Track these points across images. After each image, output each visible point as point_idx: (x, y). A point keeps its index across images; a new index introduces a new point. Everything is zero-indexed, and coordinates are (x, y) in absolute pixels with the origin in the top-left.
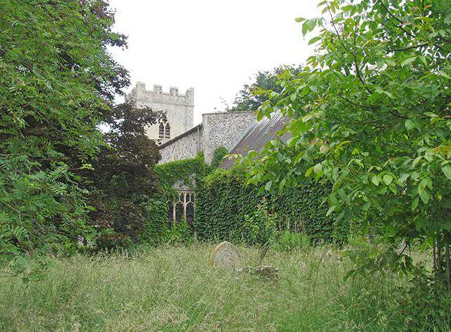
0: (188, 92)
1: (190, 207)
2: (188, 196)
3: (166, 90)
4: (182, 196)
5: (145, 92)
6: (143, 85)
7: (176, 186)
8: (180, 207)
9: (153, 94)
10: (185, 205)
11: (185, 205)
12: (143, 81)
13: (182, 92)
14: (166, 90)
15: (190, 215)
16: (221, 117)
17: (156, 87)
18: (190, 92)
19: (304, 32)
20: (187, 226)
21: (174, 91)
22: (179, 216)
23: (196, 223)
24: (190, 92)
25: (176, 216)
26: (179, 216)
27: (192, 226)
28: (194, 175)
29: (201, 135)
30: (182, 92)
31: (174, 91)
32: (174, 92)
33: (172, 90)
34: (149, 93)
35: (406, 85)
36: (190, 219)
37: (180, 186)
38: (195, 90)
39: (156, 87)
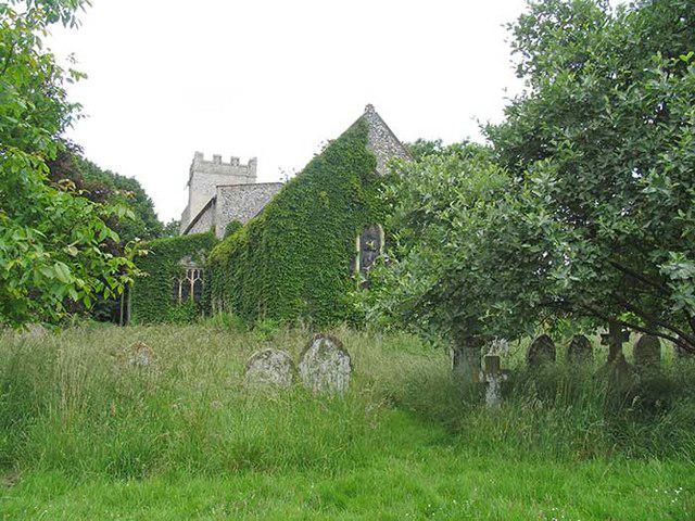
0: (250, 161)
1: (198, 284)
3: (226, 160)
4: (190, 273)
7: (183, 262)
8: (187, 286)
9: (212, 164)
10: (193, 282)
11: (193, 282)
12: (201, 151)
13: (244, 162)
14: (226, 160)
17: (215, 157)
18: (253, 162)
19: (65, 25)
20: (193, 304)
21: (235, 160)
22: (185, 294)
24: (253, 162)
25: (195, 294)
30: (244, 162)
31: (235, 160)
36: (197, 297)
37: (188, 262)
39: (215, 157)
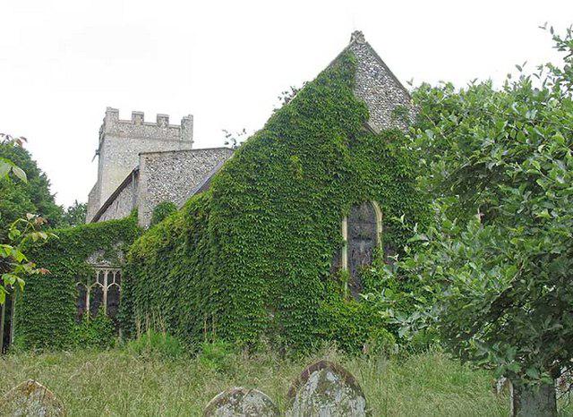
0: (183, 121)
1: (113, 292)
2: (110, 275)
3: (150, 118)
5: (118, 122)
6: (116, 112)
7: (91, 261)
8: (98, 294)
10: (105, 288)
11: (105, 288)
13: (175, 121)
14: (150, 118)
15: (113, 304)
16: (167, 158)
17: (134, 115)
18: (187, 122)
21: (161, 119)
22: (95, 305)
23: (121, 316)
26: (95, 305)
27: (115, 320)
28: (120, 244)
29: (137, 184)
30: (175, 121)
31: (138, 116)
32: (163, 122)
33: (159, 118)
34: (124, 123)
35: (294, 276)
36: (113, 309)
37: (98, 261)
38: (194, 118)
39: (134, 115)
